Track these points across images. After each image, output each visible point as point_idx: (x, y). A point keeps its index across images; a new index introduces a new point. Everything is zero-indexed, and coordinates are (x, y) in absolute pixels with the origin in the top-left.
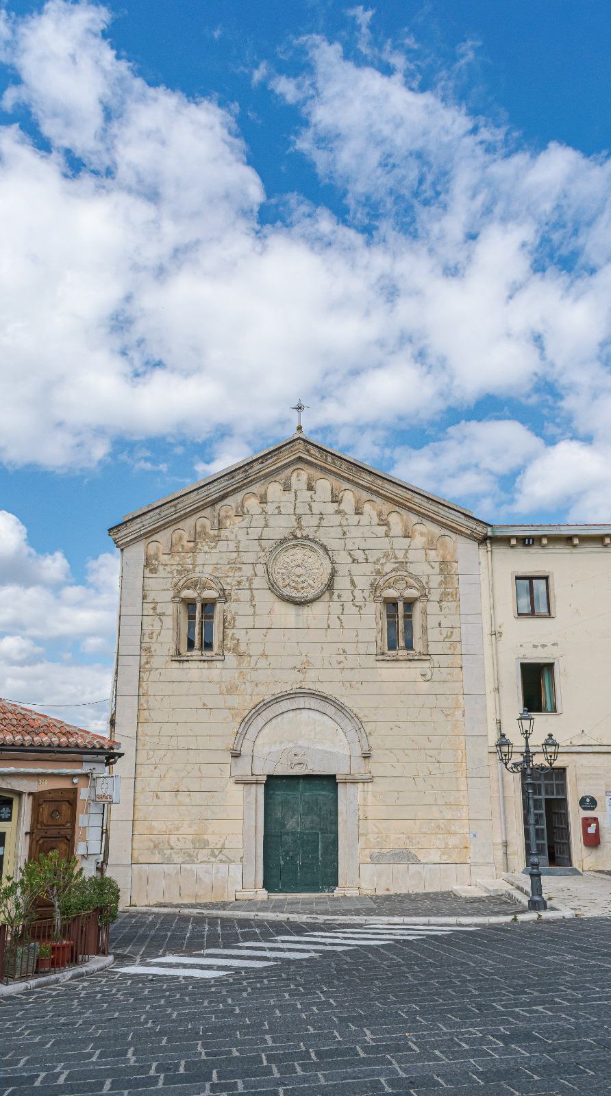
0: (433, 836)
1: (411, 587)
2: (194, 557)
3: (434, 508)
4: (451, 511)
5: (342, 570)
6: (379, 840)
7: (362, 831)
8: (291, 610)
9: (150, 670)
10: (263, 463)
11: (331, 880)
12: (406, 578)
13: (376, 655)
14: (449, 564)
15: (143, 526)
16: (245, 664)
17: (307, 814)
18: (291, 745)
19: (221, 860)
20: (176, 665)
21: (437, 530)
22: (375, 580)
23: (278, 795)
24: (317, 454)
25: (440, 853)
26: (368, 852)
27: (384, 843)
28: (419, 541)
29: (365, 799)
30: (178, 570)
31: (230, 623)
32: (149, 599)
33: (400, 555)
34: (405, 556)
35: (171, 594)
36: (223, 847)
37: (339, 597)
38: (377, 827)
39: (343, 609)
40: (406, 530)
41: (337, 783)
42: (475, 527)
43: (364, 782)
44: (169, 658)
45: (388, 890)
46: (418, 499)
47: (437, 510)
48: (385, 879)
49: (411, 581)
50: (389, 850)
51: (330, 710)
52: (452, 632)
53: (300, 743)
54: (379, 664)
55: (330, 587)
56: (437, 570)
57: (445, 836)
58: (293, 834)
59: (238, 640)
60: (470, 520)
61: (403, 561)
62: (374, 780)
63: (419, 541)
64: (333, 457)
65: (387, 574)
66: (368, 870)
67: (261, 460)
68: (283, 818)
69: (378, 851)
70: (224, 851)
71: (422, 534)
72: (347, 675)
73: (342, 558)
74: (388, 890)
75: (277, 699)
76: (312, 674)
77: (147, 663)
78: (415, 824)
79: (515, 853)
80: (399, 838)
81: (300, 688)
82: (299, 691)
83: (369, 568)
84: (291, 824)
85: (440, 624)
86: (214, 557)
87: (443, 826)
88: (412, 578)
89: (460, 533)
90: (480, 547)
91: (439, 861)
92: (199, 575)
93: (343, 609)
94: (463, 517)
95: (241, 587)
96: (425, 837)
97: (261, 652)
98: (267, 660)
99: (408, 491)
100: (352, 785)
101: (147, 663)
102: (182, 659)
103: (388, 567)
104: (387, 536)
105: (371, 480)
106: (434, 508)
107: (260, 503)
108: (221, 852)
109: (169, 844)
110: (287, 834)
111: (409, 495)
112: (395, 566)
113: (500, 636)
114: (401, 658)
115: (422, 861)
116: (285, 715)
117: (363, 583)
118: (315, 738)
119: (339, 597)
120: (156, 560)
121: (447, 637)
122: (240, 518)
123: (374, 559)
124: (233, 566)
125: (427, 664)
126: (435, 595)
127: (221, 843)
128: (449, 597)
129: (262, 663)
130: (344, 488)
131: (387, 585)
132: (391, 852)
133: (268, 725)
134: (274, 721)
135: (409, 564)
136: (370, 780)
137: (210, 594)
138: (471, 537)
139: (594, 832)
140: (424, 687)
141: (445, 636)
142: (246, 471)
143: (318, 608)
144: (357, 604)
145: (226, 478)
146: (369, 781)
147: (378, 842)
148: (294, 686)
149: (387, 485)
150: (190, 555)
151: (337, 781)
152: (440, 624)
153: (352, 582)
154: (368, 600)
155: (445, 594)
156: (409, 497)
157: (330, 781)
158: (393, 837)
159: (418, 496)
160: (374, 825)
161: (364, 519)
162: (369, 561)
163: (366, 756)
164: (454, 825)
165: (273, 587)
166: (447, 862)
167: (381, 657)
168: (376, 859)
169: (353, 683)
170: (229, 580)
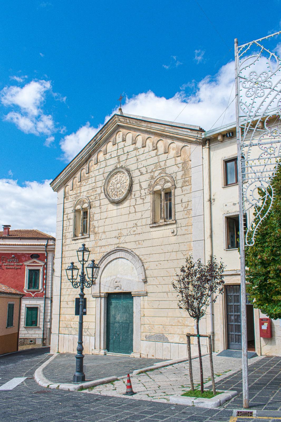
0: (176, 327)
1: (168, 182)
2: (81, 189)
3: (175, 131)
4: (184, 130)
5: (136, 181)
6: (150, 328)
7: (142, 323)
8: (115, 207)
9: (66, 245)
10: (101, 133)
11: (129, 349)
12: (165, 177)
13: (150, 225)
14: (187, 163)
15: (61, 179)
16: (97, 238)
17: (125, 313)
18: (115, 277)
19: (87, 334)
20: (74, 242)
21: (181, 144)
22: (151, 182)
23: (113, 303)
24: (123, 120)
25: (179, 337)
26: (144, 334)
27: (152, 330)
28: (172, 153)
29: (144, 305)
30: (75, 197)
31: (92, 218)
32: (66, 213)
33: (162, 164)
34: (165, 165)
35: (72, 208)
36: (88, 328)
37: (134, 195)
38: (149, 321)
39: (136, 202)
40: (165, 150)
41: (133, 297)
42: (197, 135)
43: (143, 296)
44: (71, 239)
45: (153, 356)
46: (167, 129)
47: (177, 131)
48: (152, 350)
49: (168, 179)
50: (154, 334)
51: (130, 257)
52: (188, 204)
53: (118, 276)
54: (152, 230)
55: (130, 190)
56: (181, 169)
57: (183, 327)
58: (119, 322)
59: (95, 226)
60: (194, 132)
61: (164, 167)
62: (148, 295)
63: (172, 153)
64: (130, 119)
65: (156, 177)
66: (145, 344)
67: (100, 133)
68: (115, 315)
69: (149, 334)
70: (89, 330)
71: (173, 149)
72: (138, 238)
73: (136, 174)
74: (153, 356)
75: (109, 254)
76: (122, 239)
77: (65, 242)
78: (167, 319)
79: (218, 340)
80: (159, 327)
81: (118, 247)
82: (118, 248)
83: (147, 176)
84: (118, 318)
85: (182, 201)
86: (87, 188)
87: (181, 321)
88: (167, 177)
89: (191, 142)
90: (203, 148)
91: (178, 342)
92: (81, 197)
93: (136, 202)
94: (189, 131)
95: (96, 200)
96: (171, 327)
97: (103, 231)
98: (105, 234)
99: (161, 125)
100: (138, 297)
101: (65, 242)
102: (85, 237)
103: (157, 173)
104: (157, 155)
105: (146, 125)
106: (175, 131)
107: (104, 155)
108: (87, 330)
109: (71, 326)
110: (117, 323)
111: (162, 128)
112: (159, 171)
113: (214, 202)
114: (161, 224)
115: (170, 341)
116: (113, 262)
117: (145, 185)
118: (124, 273)
119: (134, 195)
120: (68, 194)
121: (185, 208)
122: (97, 165)
123: (150, 171)
124: (94, 189)
125: (174, 226)
126: (179, 185)
127: (88, 326)
128: (187, 183)
129: (104, 236)
130: (137, 135)
131: (155, 183)
132: (156, 335)
133: (106, 268)
134: (108, 266)
135: (167, 169)
136: (146, 294)
137: (86, 205)
138: (196, 143)
139: (266, 329)
140: (173, 239)
141: (184, 207)
142: (95, 140)
143: (126, 204)
144: (142, 197)
145: (88, 146)
146: (145, 295)
147: (149, 329)
148: (115, 247)
149: (153, 126)
150: (79, 189)
151: (132, 295)
152: (182, 201)
153: (140, 186)
154: (147, 194)
155: (185, 182)
156: (163, 128)
157: (128, 295)
158: (156, 326)
159: (168, 127)
160: (148, 319)
161: (146, 149)
162: (148, 172)
163: (145, 282)
164: (187, 321)
165: (107, 196)
166: (183, 342)
167: (155, 225)
168: (148, 338)
169: (140, 242)
170: (92, 197)
